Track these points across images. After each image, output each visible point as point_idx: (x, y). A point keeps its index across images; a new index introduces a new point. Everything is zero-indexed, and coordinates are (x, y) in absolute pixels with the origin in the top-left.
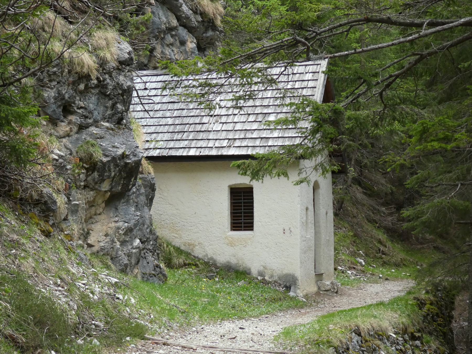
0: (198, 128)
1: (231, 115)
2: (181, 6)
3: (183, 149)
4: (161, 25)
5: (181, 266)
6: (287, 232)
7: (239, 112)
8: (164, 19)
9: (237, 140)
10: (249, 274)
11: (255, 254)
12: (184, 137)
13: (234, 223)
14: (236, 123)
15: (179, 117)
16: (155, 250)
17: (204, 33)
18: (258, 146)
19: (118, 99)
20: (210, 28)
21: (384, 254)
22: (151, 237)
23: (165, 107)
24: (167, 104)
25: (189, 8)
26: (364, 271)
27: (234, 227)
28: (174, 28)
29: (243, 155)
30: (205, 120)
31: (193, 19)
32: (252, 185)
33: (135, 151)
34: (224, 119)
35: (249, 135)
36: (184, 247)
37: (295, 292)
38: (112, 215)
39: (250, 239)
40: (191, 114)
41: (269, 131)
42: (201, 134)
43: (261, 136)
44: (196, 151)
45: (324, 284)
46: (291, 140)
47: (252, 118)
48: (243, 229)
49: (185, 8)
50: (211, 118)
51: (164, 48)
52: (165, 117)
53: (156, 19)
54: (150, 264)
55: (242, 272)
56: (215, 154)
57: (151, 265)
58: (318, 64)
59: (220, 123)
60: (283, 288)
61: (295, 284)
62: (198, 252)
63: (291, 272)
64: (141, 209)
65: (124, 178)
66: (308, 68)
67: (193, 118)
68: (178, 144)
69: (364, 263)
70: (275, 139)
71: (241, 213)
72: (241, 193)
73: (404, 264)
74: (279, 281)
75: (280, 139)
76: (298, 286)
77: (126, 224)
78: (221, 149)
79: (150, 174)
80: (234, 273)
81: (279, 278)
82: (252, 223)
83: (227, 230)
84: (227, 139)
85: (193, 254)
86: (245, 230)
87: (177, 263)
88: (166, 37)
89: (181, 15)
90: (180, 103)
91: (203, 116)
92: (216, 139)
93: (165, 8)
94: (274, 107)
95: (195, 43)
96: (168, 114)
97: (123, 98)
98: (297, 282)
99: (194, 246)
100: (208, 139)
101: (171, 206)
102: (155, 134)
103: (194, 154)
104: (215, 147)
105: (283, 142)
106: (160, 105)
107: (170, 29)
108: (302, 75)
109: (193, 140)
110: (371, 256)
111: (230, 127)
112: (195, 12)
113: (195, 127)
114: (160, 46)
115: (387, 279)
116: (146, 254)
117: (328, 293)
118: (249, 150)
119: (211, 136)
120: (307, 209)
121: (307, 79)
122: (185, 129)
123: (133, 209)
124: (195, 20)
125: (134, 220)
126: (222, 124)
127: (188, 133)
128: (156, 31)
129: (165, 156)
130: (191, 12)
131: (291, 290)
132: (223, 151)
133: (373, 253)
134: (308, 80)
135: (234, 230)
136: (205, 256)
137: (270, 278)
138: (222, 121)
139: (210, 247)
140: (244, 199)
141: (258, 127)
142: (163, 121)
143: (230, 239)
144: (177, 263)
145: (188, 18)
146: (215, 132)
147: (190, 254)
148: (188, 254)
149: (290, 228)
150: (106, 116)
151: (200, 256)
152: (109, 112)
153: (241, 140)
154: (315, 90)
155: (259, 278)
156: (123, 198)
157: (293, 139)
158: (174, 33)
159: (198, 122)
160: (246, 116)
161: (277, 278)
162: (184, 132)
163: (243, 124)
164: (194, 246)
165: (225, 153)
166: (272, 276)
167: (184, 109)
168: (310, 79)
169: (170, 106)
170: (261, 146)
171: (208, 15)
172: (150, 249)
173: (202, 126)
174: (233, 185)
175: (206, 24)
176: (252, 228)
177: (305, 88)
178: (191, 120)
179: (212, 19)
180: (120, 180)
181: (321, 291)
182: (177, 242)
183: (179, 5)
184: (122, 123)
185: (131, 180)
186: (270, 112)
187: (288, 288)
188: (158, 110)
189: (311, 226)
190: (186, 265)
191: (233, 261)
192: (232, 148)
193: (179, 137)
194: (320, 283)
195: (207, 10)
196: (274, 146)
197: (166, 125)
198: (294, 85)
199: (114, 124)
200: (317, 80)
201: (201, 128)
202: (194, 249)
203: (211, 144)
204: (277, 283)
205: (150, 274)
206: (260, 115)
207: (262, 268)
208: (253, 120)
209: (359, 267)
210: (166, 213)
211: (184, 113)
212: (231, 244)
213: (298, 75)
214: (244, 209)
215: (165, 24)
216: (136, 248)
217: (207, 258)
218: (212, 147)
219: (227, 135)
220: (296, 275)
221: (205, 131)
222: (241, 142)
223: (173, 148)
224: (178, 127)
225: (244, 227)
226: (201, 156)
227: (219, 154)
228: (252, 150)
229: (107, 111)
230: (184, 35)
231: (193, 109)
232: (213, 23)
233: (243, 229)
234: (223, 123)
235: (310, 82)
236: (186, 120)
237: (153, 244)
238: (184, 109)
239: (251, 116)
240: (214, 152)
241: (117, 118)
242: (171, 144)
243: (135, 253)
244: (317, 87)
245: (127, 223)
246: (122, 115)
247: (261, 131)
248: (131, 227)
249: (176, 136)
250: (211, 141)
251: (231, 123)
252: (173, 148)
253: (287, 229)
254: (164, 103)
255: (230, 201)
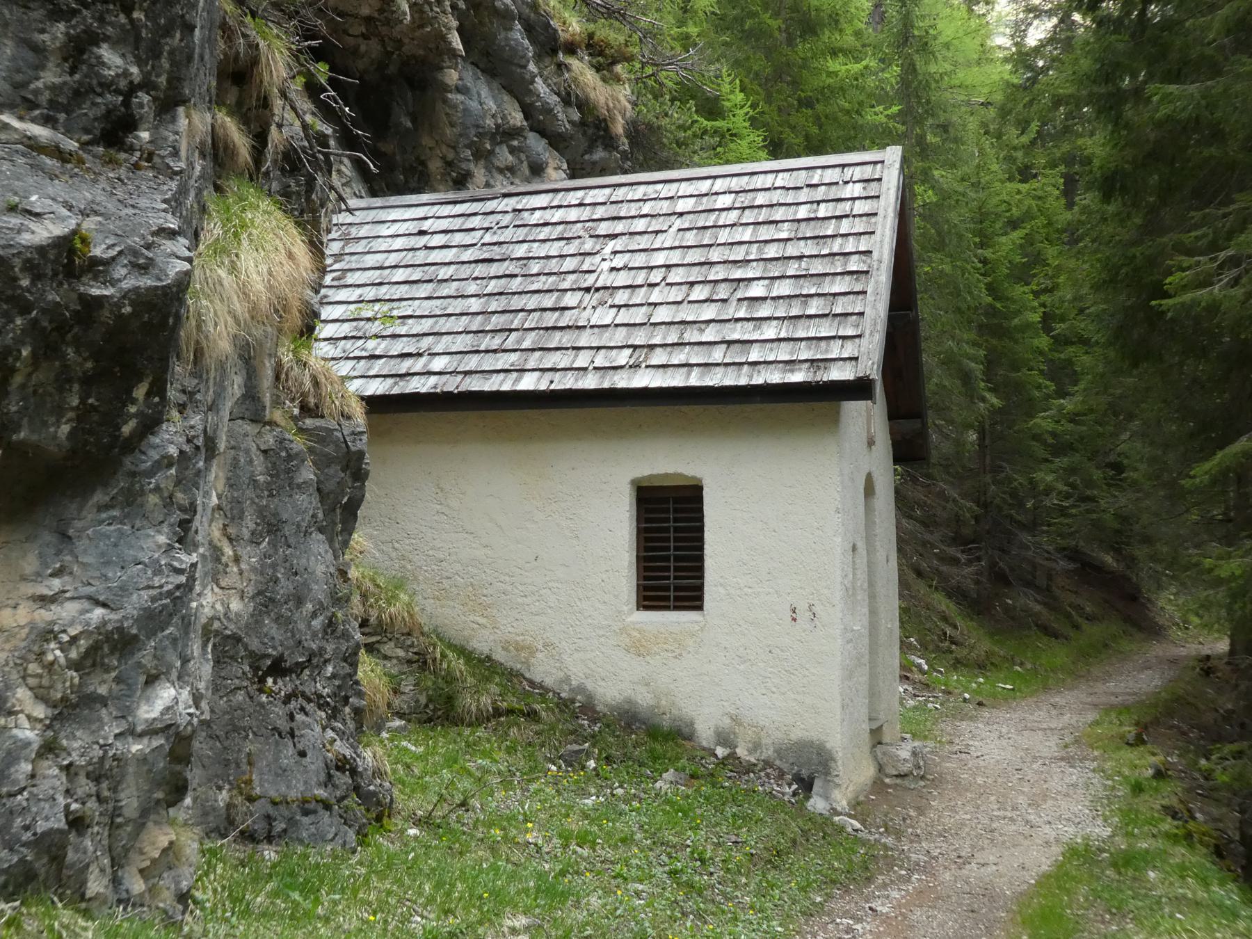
0: (550, 319)
1: (641, 286)
2: (533, 82)
3: (502, 375)
4: (483, 117)
5: (481, 719)
6: (803, 615)
7: (664, 279)
8: (491, 105)
9: (659, 350)
10: (690, 737)
11: (706, 678)
12: (509, 344)
13: (646, 588)
14: (655, 305)
15: (501, 294)
16: (346, 699)
17: (586, 152)
18: (718, 365)
19: (101, 20)
20: (599, 143)
21: (953, 642)
22: (330, 648)
23: (465, 271)
24: (473, 265)
25: (552, 90)
26: (927, 685)
27: (646, 598)
28: (515, 133)
29: (674, 388)
30: (570, 299)
31: (560, 116)
32: (700, 480)
33: (148, 247)
34: (622, 297)
35: (692, 335)
36: (503, 653)
37: (827, 798)
38: (30, 564)
39: (692, 635)
40: (534, 287)
41: (751, 325)
42: (558, 334)
43: (728, 338)
44: (539, 379)
45: (896, 759)
46: (817, 347)
47: (699, 293)
48: (672, 603)
49: (540, 86)
50: (587, 297)
51: (492, 177)
52: (463, 296)
53: (474, 105)
54: (308, 759)
55: (669, 734)
56: (592, 387)
57: (314, 764)
58: (875, 163)
59: (611, 306)
60: (790, 785)
61: (827, 773)
62: (543, 670)
63: (813, 735)
64: (292, 541)
65: (88, 382)
66: (848, 172)
67: (536, 296)
68: (489, 363)
69: (926, 667)
70: (768, 345)
71: (667, 559)
72: (666, 501)
73: (992, 664)
74: (778, 762)
75: (783, 344)
76: (836, 780)
77: (99, 612)
78: (612, 372)
79: (349, 418)
80: (645, 740)
81: (778, 752)
82: (700, 588)
83: (625, 608)
84: (629, 347)
85: (527, 675)
86: (677, 608)
87: (473, 708)
88: (497, 150)
89: (532, 104)
90: (507, 263)
91: (566, 290)
92: (598, 348)
93: (495, 85)
94: (761, 263)
95: (564, 171)
96: (472, 288)
97: (132, 21)
98: (833, 765)
99: (532, 651)
100: (574, 348)
101: (470, 537)
102: (431, 338)
103: (531, 388)
104: (595, 368)
105: (791, 353)
106: (453, 267)
107: (506, 134)
108: (834, 187)
109: (533, 350)
110: (931, 647)
111: (638, 316)
112: (566, 101)
113: (540, 318)
114: (483, 171)
115: (980, 704)
116: (300, 717)
117: (906, 782)
118: (694, 374)
119: (585, 339)
120: (854, 548)
121: (848, 196)
122: (512, 322)
123: (162, 539)
124: (565, 118)
125: (145, 595)
126: (615, 310)
127: (521, 333)
128: (473, 131)
129: (451, 393)
130: (556, 98)
131: (816, 788)
132: (616, 378)
133: (933, 640)
134: (853, 199)
135: (647, 608)
136: (562, 681)
137: (750, 752)
138: (617, 302)
139: (576, 655)
140: (676, 520)
141: (718, 314)
142: (457, 306)
143: (635, 634)
144: (473, 708)
145: (548, 111)
146: (596, 330)
147: (519, 675)
148: (511, 676)
149: (811, 606)
150: (37, 92)
151: (549, 682)
152: (51, 76)
153: (669, 349)
154: (873, 220)
155: (721, 752)
156: (105, 485)
157: (823, 344)
158: (515, 143)
159: (549, 306)
160: (685, 288)
161: (770, 752)
162: (511, 330)
163: (674, 307)
164: (532, 651)
165: (621, 384)
166: (756, 747)
167: (516, 276)
168: (856, 195)
169: (480, 270)
170: (727, 365)
171: (595, 108)
172: (320, 696)
173: (561, 315)
174: (644, 478)
175: (590, 131)
176: (698, 603)
177: (847, 216)
178: (532, 302)
179: (605, 120)
180: (61, 390)
181: (887, 776)
182: (482, 643)
183: (528, 77)
184: (130, 140)
185: (129, 392)
186: (750, 275)
187: (806, 785)
188: (446, 281)
189: (862, 596)
190: (500, 715)
191: (644, 699)
192: (641, 371)
193: (496, 342)
194: (884, 754)
195: (592, 95)
196: (765, 362)
197: (462, 314)
198: (815, 211)
199: (86, 138)
200: (878, 197)
201: (556, 321)
202: (533, 660)
203: (582, 360)
204: (771, 767)
205: (305, 801)
206: (723, 285)
207: (727, 721)
208: (702, 298)
209: (918, 676)
210: (454, 558)
211: (515, 284)
212: (638, 648)
213: (823, 187)
214: (676, 549)
215: (493, 116)
216: (151, 732)
217: (566, 688)
218: (585, 369)
219: (628, 336)
220: (828, 746)
221: (569, 327)
222: (670, 354)
223: (476, 372)
224: (494, 318)
225: (677, 599)
226: (553, 391)
227: (606, 385)
228: (702, 377)
229: (42, 67)
230: (540, 149)
231: (538, 275)
232: (607, 129)
233: (672, 603)
234: (619, 307)
235: (857, 202)
236: (517, 303)
237: (334, 676)
238: (516, 276)
239: (697, 288)
240: (590, 382)
241: (100, 111)
242: (472, 362)
243: (142, 759)
244: (881, 213)
245: (104, 605)
246: (126, 103)
247: (728, 325)
248: (120, 630)
249: (486, 342)
250: (582, 352)
251: (642, 305)
252: (476, 372)
253: (802, 606)
254: (463, 263)
255: (635, 524)
